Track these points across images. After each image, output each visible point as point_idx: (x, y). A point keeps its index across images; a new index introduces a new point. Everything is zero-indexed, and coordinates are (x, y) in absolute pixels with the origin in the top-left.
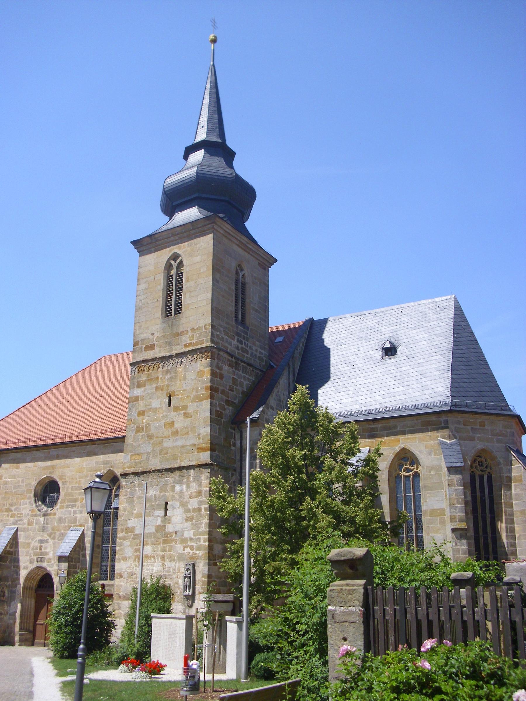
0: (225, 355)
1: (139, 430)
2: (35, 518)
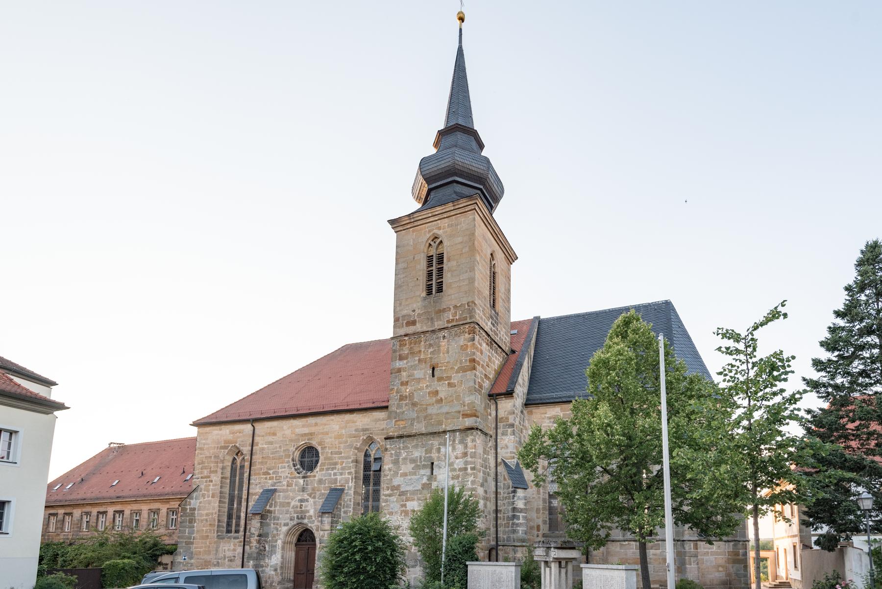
0: (484, 334)
1: (402, 398)
2: (294, 480)
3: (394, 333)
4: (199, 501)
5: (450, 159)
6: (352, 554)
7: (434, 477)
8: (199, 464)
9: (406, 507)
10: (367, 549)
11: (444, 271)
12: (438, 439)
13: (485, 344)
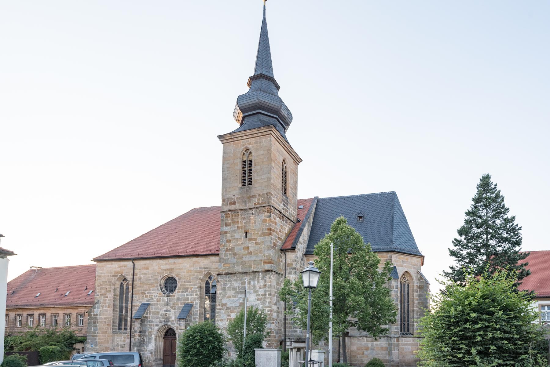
0: (277, 212)
1: (227, 250)
2: (162, 298)
4: (100, 310)
5: (255, 99)
6: (195, 344)
8: (98, 286)
9: (230, 317)
10: (203, 341)
11: (252, 171)
12: (249, 276)
13: (278, 218)
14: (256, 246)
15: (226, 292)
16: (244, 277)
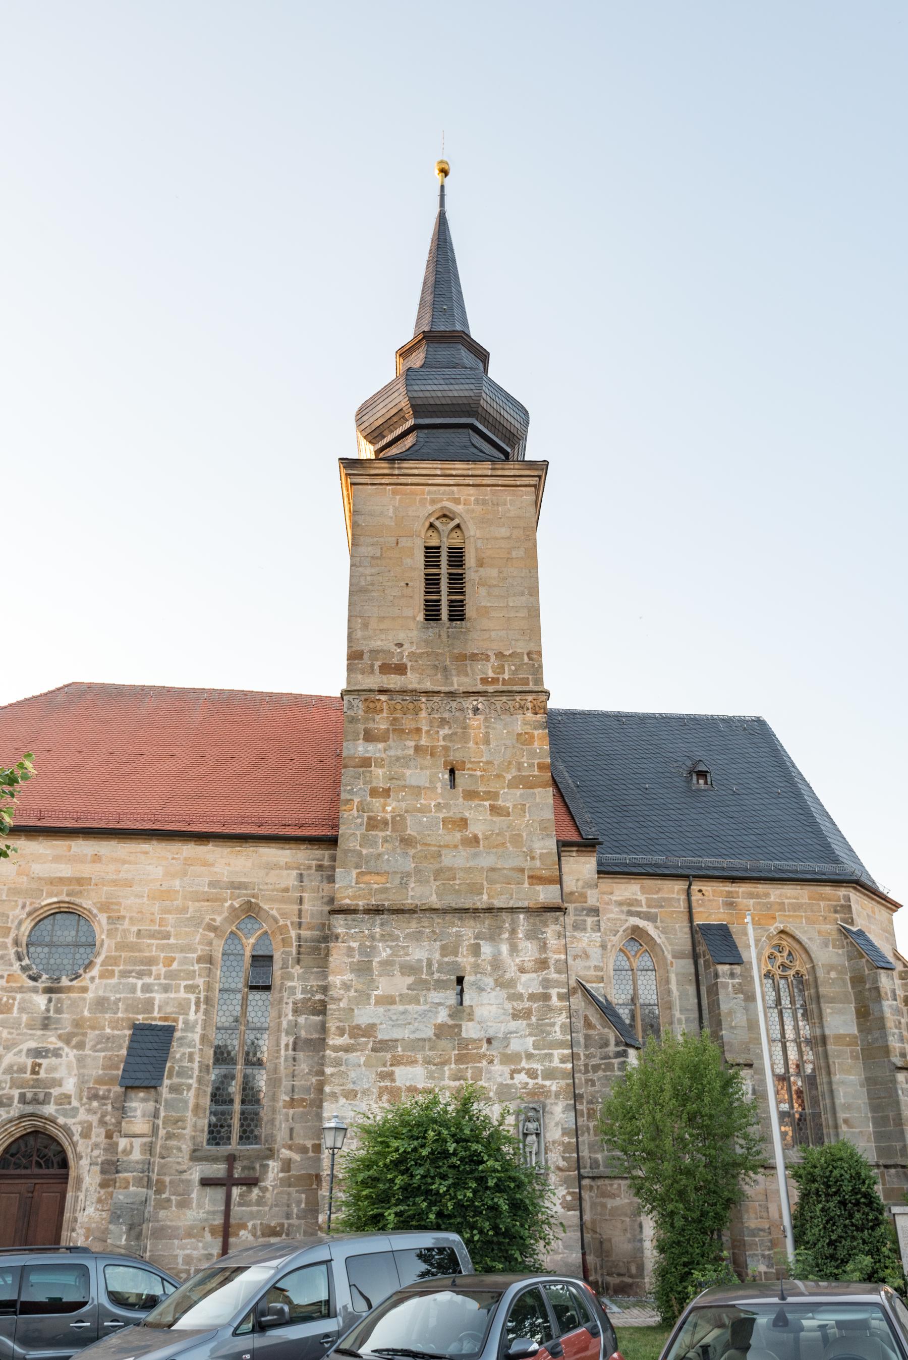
2: (19, 996)
3: (348, 683)
7: (468, 1010)
9: (393, 1080)
12: (472, 923)
14: (495, 819)
15: (373, 981)
16: (453, 925)
